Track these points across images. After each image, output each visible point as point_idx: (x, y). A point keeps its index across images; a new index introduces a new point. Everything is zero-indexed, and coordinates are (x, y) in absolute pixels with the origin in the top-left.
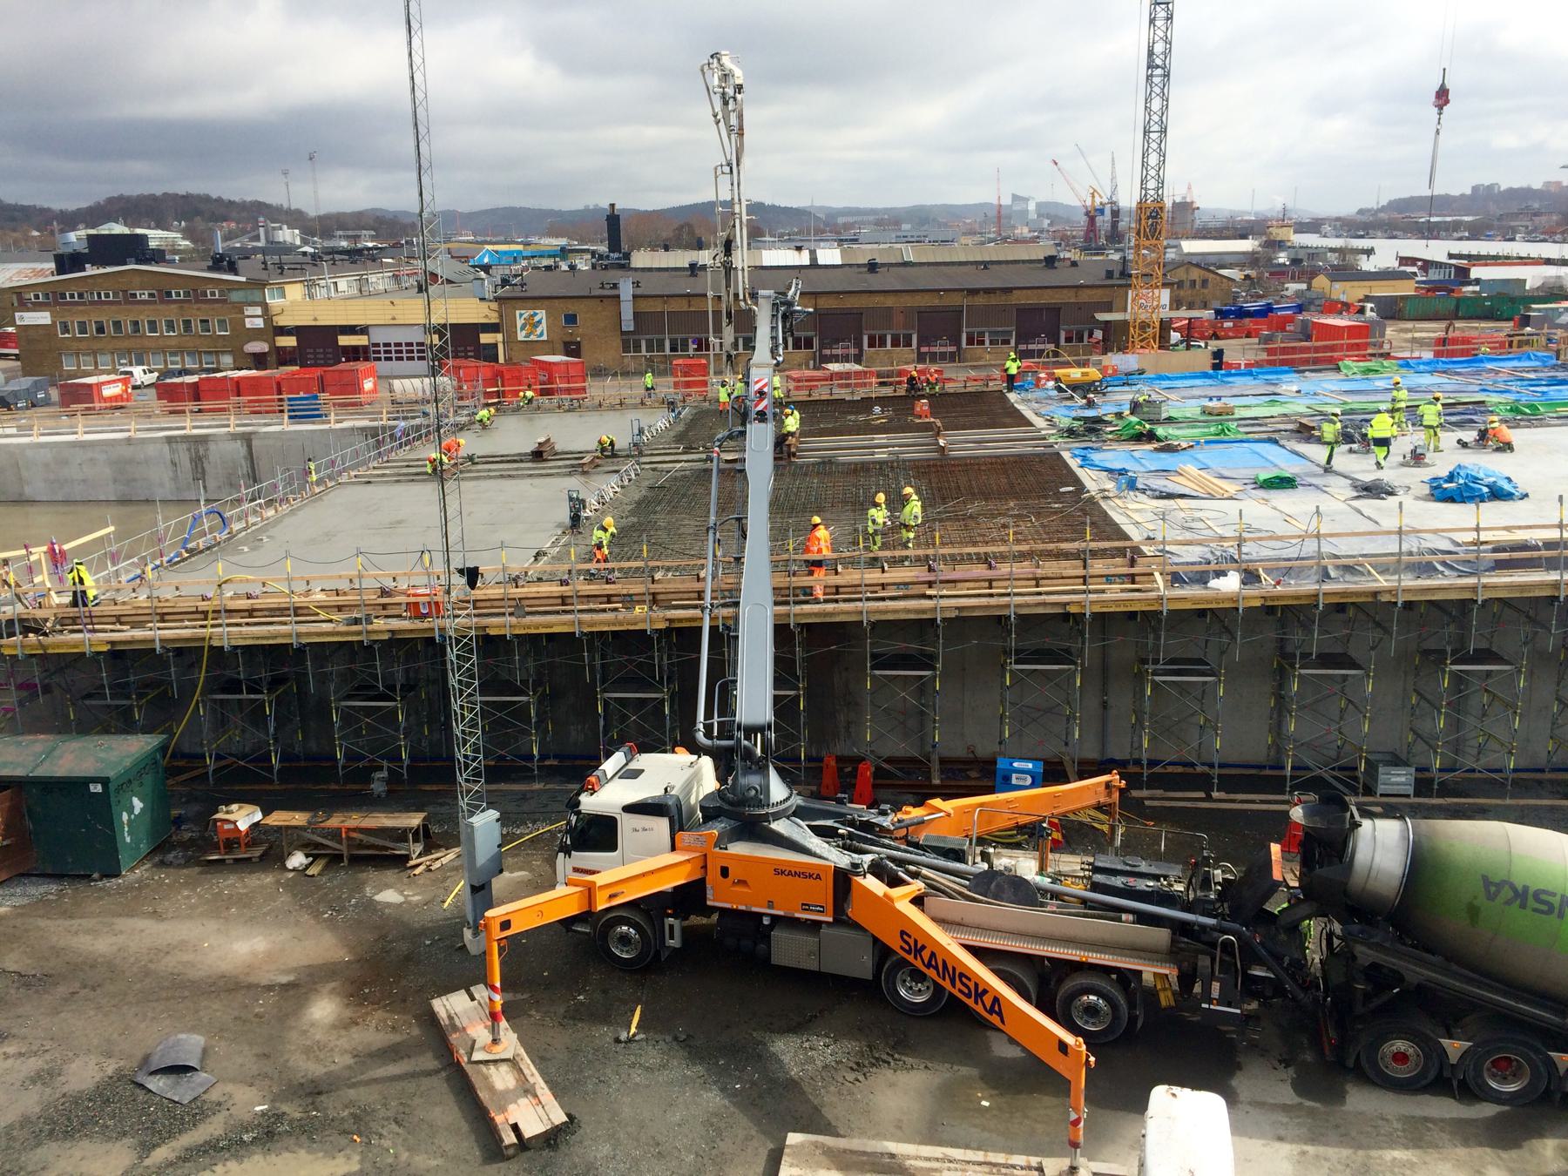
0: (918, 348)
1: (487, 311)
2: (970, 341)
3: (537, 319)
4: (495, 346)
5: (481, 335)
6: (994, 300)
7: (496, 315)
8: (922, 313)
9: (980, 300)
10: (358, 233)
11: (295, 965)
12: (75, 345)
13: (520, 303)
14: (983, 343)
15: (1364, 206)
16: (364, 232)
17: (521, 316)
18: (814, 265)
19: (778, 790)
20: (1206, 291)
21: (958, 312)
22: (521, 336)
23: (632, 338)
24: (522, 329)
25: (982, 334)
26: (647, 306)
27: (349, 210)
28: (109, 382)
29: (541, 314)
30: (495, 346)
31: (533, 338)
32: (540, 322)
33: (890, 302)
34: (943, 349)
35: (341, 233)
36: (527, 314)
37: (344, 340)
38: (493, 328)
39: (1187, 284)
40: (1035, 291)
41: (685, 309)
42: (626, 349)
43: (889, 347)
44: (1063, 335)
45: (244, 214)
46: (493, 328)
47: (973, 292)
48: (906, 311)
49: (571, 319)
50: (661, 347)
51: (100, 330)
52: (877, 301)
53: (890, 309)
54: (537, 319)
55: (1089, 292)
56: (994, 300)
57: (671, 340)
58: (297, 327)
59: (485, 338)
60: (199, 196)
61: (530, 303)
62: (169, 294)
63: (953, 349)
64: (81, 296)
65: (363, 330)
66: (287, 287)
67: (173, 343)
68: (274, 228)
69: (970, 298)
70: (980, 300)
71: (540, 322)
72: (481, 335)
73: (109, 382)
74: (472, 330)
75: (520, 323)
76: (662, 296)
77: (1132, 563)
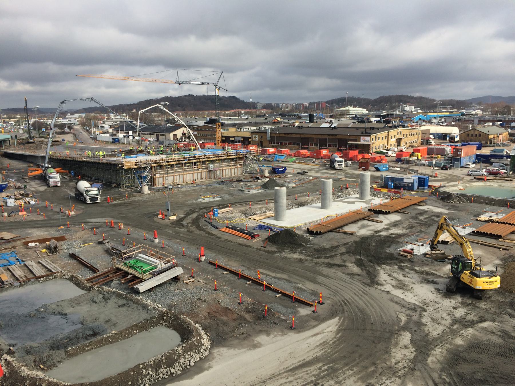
6: (333, 137)
8: (320, 139)
9: (331, 137)
16: (449, 106)
17: (254, 136)
18: (330, 127)
19: (105, 336)
20: (480, 138)
21: (326, 139)
22: (254, 140)
25: (331, 145)
26: (273, 135)
29: (257, 136)
33: (313, 136)
36: (255, 135)
37: (231, 139)
39: (474, 135)
46: (250, 138)
47: (329, 135)
48: (317, 139)
49: (262, 137)
50: (287, 144)
55: (352, 136)
65: (234, 137)
68: (405, 106)
70: (331, 137)
75: (257, 138)
77: (4, 121)
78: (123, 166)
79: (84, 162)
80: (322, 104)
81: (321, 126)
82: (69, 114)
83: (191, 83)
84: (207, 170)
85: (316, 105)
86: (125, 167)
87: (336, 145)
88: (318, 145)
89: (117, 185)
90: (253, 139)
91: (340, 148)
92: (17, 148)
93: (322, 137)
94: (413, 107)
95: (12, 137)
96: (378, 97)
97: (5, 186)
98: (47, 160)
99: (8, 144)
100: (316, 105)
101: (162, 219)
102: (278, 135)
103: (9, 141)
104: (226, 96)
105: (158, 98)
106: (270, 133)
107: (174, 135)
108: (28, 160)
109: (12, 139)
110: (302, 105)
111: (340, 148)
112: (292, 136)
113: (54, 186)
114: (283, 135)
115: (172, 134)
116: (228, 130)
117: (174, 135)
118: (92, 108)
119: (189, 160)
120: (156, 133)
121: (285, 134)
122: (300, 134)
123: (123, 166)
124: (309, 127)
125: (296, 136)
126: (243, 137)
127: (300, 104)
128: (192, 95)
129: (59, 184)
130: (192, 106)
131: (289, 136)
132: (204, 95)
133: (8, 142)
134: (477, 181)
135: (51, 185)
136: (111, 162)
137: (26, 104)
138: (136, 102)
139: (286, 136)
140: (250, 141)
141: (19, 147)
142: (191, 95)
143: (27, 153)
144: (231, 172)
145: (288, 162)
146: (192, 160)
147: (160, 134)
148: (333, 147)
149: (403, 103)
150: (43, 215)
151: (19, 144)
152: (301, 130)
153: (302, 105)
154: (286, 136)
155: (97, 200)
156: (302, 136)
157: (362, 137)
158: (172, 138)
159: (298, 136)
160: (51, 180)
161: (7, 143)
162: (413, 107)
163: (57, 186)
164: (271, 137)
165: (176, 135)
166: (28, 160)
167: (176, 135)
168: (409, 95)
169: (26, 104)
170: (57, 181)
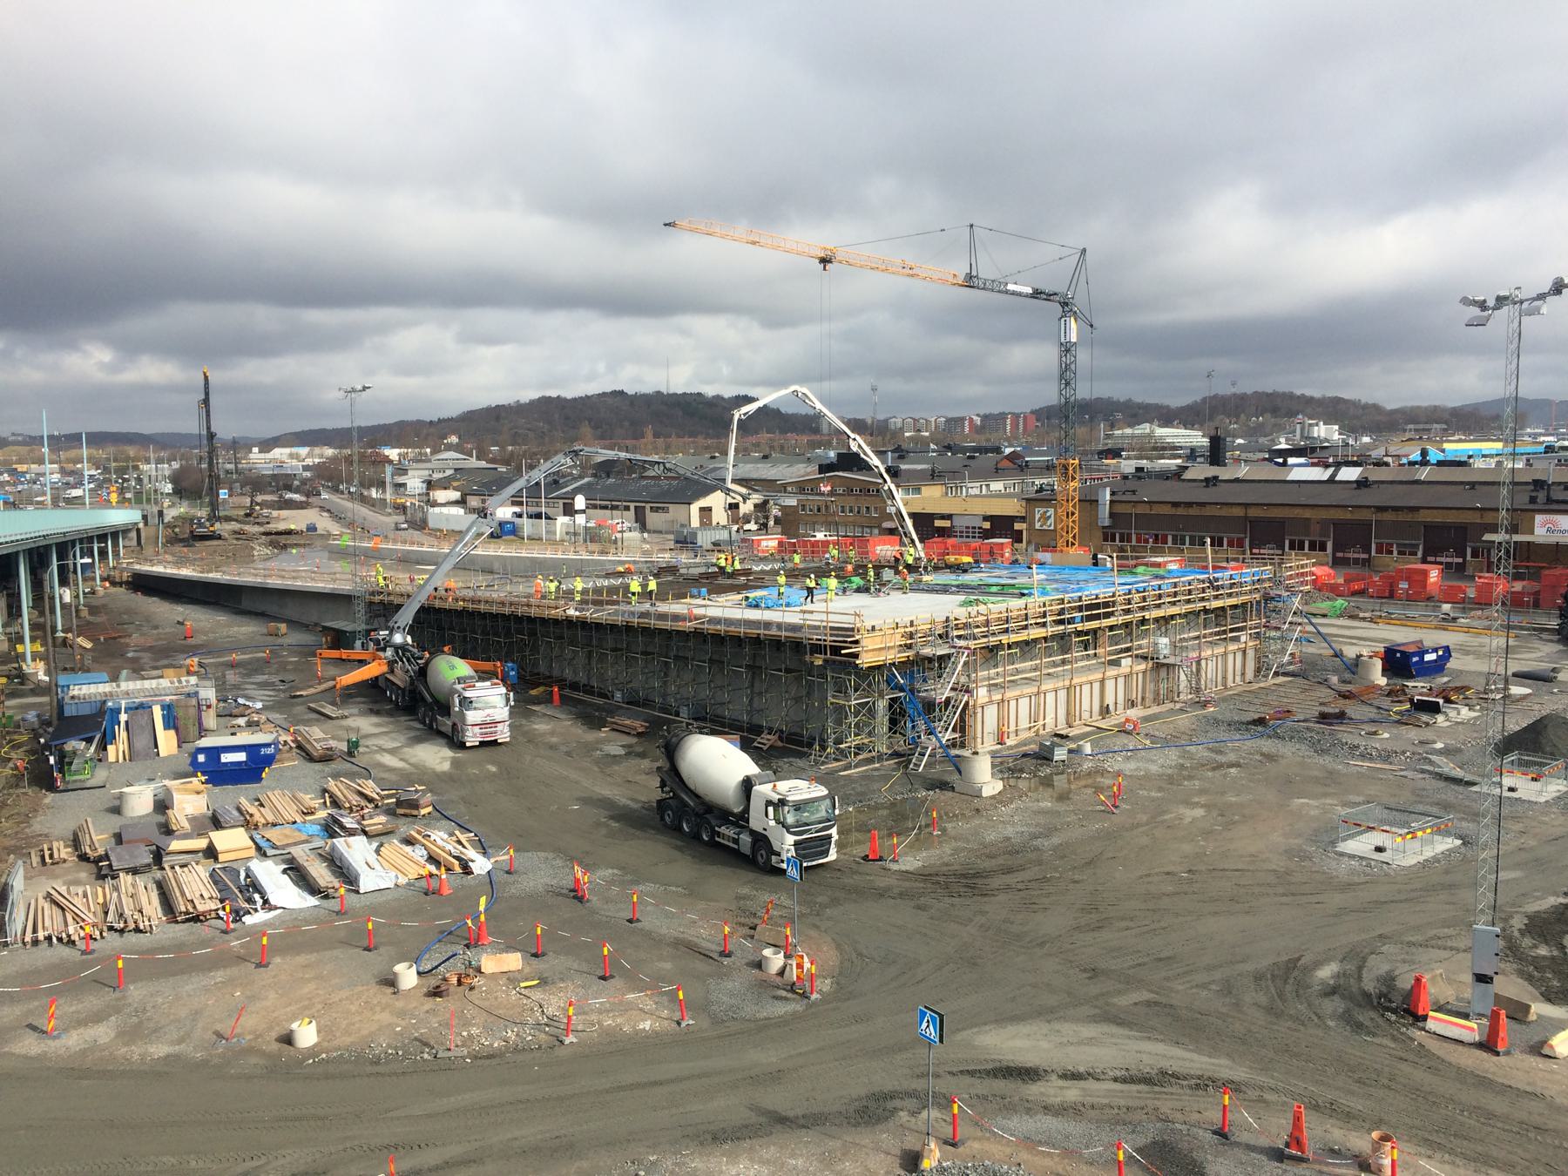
0: (1334, 554)
1: (1019, 508)
2: (1379, 551)
3: (1048, 514)
4: (1021, 531)
5: (989, 527)
6: (1402, 517)
7: (1024, 511)
8: (1338, 525)
9: (1388, 516)
10: (1428, 426)
11: (771, 1108)
12: (807, 518)
13: (1039, 503)
14: (1391, 552)
15: (22, 512)
16: (1435, 426)
17: (1038, 512)
18: (1331, 480)
23: (1110, 531)
24: (1039, 521)
26: (1119, 509)
27: (1425, 404)
28: (1171, 561)
30: (1021, 531)
31: (1045, 527)
32: (1050, 517)
33: (1307, 514)
34: (1356, 556)
35: (1412, 426)
37: (938, 523)
38: (1023, 519)
40: (1440, 511)
41: (1148, 512)
42: (1105, 540)
43: (1306, 550)
44: (1469, 551)
45: (1320, 410)
46: (1023, 519)
48: (1324, 523)
50: (1129, 540)
51: (819, 510)
52: (1297, 512)
53: (1308, 519)
54: (1048, 514)
56: (1402, 517)
57: (1377, 544)
58: (991, 516)
59: (1017, 526)
60: (1284, 394)
61: (1045, 503)
62: (852, 491)
63: (1460, 560)
64: (812, 490)
65: (949, 517)
66: (923, 488)
67: (851, 519)
68: (1310, 425)
69: (1379, 514)
70: (1388, 516)
71: (1050, 517)
72: (989, 527)
73: (1171, 561)
74: (1011, 519)
76: (1217, 504)
78: (856, 656)
79: (569, 622)
80: (1025, 418)
81: (1290, 478)
82: (255, 450)
83: (1011, 287)
84: (1150, 664)
85: (1008, 421)
86: (866, 660)
87: (1417, 546)
88: (1247, 542)
89: (780, 738)
90: (1031, 524)
91: (1340, 555)
92: (169, 557)
93: (1349, 516)
94: (1336, 427)
95: (145, 517)
96: (1198, 398)
97: (271, 750)
98: (406, 617)
99: (134, 542)
100: (1008, 421)
101: (1480, 1046)
102: (1140, 510)
103: (138, 530)
104: (726, 396)
105: (522, 401)
106: (1111, 501)
107: (702, 509)
108: (246, 604)
109: (146, 524)
110: (967, 423)
111: (1340, 555)
112: (1208, 511)
113: (483, 744)
114: (1167, 510)
115: (695, 508)
116: (918, 490)
117: (702, 509)
118: (311, 432)
119: (1090, 618)
120: (632, 505)
121: (1175, 505)
122: (1246, 505)
123: (856, 656)
124: (1237, 480)
125: (1225, 512)
126: (986, 518)
127: (962, 419)
128: (622, 393)
129: (503, 734)
130: (626, 424)
131: (1193, 511)
132: (658, 393)
133: (134, 534)
134: (1399, 645)
135: (472, 737)
136: (721, 628)
137: (207, 394)
138: (453, 411)
139: (1180, 511)
140: (1020, 532)
141: (173, 555)
142: (620, 394)
143: (186, 572)
144: (1225, 671)
145: (1324, 616)
146: (1097, 617)
147: (648, 506)
148: (1400, 553)
149: (1304, 415)
150: (673, 994)
151: (174, 540)
152: (1212, 489)
153: (967, 423)
154: (1180, 511)
155: (826, 853)
156: (1253, 512)
157: (1539, 518)
158: (695, 523)
159: (1238, 512)
160: (472, 716)
161: (131, 540)
162: (1336, 427)
163: (495, 743)
164: (1112, 515)
165: (709, 509)
166: (246, 604)
167: (709, 509)
168: (1298, 392)
169: (207, 394)
170: (498, 718)
